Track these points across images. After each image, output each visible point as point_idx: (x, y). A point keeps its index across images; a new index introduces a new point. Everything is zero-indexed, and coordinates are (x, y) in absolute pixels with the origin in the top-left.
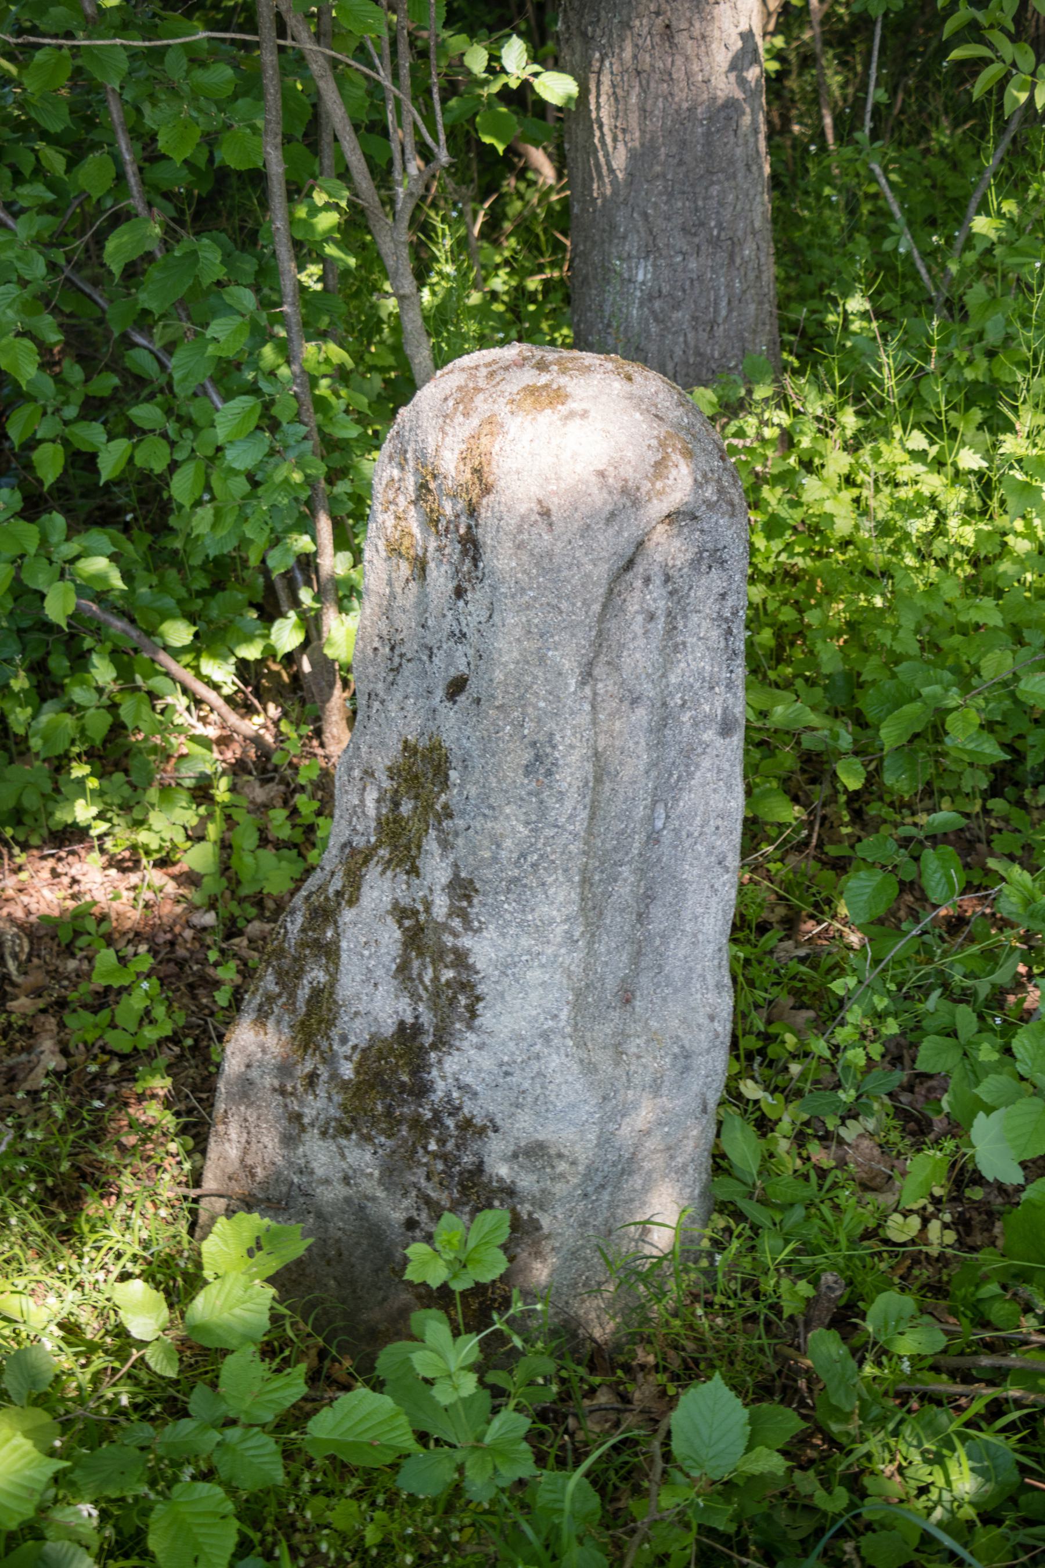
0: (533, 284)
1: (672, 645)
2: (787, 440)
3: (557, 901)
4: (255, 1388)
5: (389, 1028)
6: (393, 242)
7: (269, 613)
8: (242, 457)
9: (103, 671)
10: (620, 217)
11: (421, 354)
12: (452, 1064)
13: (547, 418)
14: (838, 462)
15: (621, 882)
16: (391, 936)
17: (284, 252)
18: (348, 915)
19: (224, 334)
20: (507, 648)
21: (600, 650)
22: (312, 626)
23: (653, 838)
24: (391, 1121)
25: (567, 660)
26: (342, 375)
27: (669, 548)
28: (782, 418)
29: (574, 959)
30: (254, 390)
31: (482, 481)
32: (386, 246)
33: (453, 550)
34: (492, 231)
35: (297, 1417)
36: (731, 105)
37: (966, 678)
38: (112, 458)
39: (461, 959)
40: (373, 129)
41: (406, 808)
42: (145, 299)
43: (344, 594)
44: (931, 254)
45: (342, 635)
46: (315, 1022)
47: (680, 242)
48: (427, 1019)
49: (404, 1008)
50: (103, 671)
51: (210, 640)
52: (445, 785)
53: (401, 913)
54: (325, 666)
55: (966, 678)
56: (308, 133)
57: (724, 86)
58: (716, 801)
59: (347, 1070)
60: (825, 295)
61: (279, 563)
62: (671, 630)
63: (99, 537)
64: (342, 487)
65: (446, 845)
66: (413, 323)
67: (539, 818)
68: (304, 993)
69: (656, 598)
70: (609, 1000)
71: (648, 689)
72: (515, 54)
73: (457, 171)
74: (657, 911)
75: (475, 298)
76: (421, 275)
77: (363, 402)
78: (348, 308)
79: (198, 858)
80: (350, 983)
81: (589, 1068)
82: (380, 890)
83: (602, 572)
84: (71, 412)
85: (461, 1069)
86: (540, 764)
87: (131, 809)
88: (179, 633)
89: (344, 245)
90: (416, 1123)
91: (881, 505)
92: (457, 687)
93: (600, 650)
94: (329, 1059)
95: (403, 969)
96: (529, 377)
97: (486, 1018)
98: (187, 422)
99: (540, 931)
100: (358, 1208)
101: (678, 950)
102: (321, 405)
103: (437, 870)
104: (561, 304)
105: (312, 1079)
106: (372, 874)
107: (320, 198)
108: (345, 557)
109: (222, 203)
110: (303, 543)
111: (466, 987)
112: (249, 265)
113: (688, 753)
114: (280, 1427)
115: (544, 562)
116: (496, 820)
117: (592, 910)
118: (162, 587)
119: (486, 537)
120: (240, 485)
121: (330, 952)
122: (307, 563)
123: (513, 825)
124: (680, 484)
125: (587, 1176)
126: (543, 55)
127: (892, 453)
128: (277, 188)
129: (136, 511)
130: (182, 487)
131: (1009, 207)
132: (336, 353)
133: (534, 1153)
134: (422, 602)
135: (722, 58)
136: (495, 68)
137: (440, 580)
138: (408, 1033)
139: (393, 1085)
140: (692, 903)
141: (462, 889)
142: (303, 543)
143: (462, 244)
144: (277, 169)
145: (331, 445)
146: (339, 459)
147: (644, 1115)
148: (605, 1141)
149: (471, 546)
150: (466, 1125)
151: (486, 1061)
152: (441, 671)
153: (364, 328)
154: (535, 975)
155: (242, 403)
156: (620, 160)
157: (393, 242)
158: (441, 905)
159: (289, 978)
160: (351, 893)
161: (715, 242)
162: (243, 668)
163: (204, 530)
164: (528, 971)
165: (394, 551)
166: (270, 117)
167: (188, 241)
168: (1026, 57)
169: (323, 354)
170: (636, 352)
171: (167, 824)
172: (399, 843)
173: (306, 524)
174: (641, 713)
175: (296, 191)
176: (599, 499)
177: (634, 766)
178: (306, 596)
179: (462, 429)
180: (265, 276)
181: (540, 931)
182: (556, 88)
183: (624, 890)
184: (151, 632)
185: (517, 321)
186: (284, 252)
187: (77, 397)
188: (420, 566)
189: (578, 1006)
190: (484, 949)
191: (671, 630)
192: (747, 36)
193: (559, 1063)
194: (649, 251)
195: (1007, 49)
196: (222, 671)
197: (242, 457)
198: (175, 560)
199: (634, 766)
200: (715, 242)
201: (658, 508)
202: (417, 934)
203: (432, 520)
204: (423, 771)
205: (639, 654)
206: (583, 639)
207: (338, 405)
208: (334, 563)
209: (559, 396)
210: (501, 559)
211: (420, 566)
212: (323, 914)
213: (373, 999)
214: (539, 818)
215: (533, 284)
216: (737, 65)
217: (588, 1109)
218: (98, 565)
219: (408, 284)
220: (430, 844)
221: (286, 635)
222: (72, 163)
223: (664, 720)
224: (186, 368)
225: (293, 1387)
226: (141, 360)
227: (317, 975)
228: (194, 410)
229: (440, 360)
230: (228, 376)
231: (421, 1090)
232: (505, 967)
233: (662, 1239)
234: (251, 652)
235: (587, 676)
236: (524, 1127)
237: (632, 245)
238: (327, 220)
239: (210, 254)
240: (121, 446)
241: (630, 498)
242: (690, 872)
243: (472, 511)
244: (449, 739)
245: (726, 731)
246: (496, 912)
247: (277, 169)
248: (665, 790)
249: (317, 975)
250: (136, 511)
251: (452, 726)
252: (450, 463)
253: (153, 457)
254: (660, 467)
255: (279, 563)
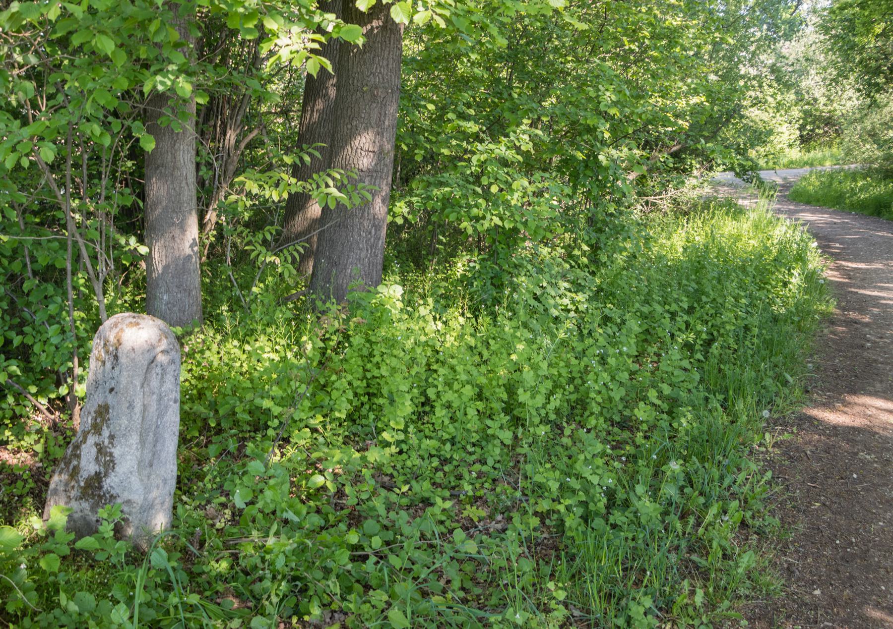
0: (138, 298)
1: (162, 382)
2: (204, 341)
3: (134, 439)
4: (62, 537)
5: (93, 473)
6: (98, 287)
7: (58, 384)
8: (55, 340)
9: (11, 399)
10: (160, 282)
11: (103, 315)
12: (108, 481)
13: (135, 329)
14: (215, 347)
15: (150, 437)
16: (94, 450)
17: (70, 289)
18: (83, 446)
19: (53, 309)
20: (124, 381)
21: (145, 381)
22: (71, 388)
23: (157, 427)
24: (93, 495)
25: (137, 382)
26: (82, 320)
27: (162, 358)
28: (202, 336)
29: (138, 454)
30: (59, 323)
31: (119, 342)
32: (96, 288)
33: (112, 358)
34: (125, 283)
35: (74, 542)
36: (190, 256)
37: (241, 400)
38: (17, 341)
39: (111, 454)
40: (94, 258)
41: (99, 420)
42: (31, 299)
43: (81, 379)
44: (244, 296)
45: (81, 389)
46: (75, 473)
47: (176, 290)
48: (102, 470)
49: (97, 468)
50: (11, 399)
51: (41, 392)
52: (108, 413)
53: (97, 445)
54: (74, 399)
55: (241, 400)
56: (77, 258)
57: (188, 251)
58: (173, 419)
59: (82, 484)
60: (216, 306)
61: (63, 369)
62: (162, 378)
63: (13, 361)
64: (81, 350)
65: (108, 427)
66: (102, 308)
67: (130, 419)
68: (71, 467)
69: (159, 370)
70: (148, 465)
71: (156, 391)
72: (133, 241)
73: (117, 269)
74: (158, 444)
75: (119, 302)
76: (105, 293)
77: (88, 328)
78: (83, 303)
79: (39, 448)
80: (83, 462)
81: (141, 480)
82: (92, 440)
83: (146, 363)
84: (6, 328)
85: (110, 482)
86: (131, 406)
87: (19, 437)
88: (33, 389)
89: (86, 286)
90: (99, 496)
91: (226, 359)
92: (112, 390)
93: (145, 381)
94: (78, 482)
95: (97, 458)
96: (131, 320)
97: (117, 469)
98: (39, 332)
99: (130, 446)
100: (84, 518)
101: (163, 455)
102: (77, 328)
103: (106, 433)
104: (142, 305)
105: (73, 487)
106: (90, 436)
107: (80, 275)
108: (81, 369)
109: (52, 275)
110: (70, 364)
111: (112, 461)
112: (61, 291)
113: (166, 407)
114: (69, 544)
115: (133, 360)
116: (121, 420)
117: (142, 442)
118: (28, 377)
119: (120, 355)
120: (53, 348)
121: (78, 457)
122: (71, 371)
123: (124, 421)
124: (164, 345)
125: (141, 507)
126: (141, 240)
127: (229, 346)
128: (69, 273)
129: (24, 354)
130: (37, 349)
131: (262, 285)
132: (83, 315)
133: (128, 502)
134: (104, 371)
135: (187, 245)
136: (127, 244)
137: (108, 365)
138: (98, 474)
139: (93, 489)
140: (167, 443)
141: (112, 437)
142: (70, 364)
143: (116, 287)
144: (69, 268)
145: (78, 338)
146: (82, 342)
147: (155, 493)
148: (145, 499)
149: (116, 357)
150: (112, 496)
151: (117, 480)
152: (108, 387)
153: (88, 309)
154: (129, 457)
155: (56, 326)
156: (160, 268)
157: (98, 287)
158: (106, 441)
159: (67, 464)
160: (84, 441)
161: (185, 290)
162: (50, 401)
163: (43, 359)
164: (127, 455)
165: (97, 359)
166: (68, 255)
167: (45, 285)
168: (264, 250)
169: (78, 314)
170: (163, 318)
171: (28, 441)
172: (97, 428)
173: (71, 359)
174: (155, 397)
175: (74, 274)
176: (146, 347)
177: (153, 408)
178: (69, 380)
179: (115, 331)
180: (65, 294)
181: (130, 446)
182: (143, 250)
183: (151, 437)
184: (26, 388)
185: (133, 307)
186: (70, 289)
187: (8, 324)
188: (104, 363)
189: (139, 465)
190: (117, 452)
191: (162, 378)
192: (194, 239)
193: (135, 479)
194: (167, 291)
195: (259, 248)
196: (44, 401)
197: (55, 340)
198: (31, 370)
199: (153, 408)
200: (185, 290)
201: (159, 349)
202: (101, 450)
203: (107, 352)
204: (103, 411)
205: (154, 383)
206: (141, 378)
207: (82, 328)
208: (78, 371)
209: (138, 324)
210: (123, 360)
211: (104, 363)
212: (77, 447)
213: (88, 465)
214: (130, 419)
215: (138, 298)
216: (191, 246)
217: (141, 491)
218: (14, 369)
219: (101, 297)
220: (105, 427)
221: (63, 390)
222: (10, 263)
223: (160, 399)
224: (39, 317)
225: (72, 536)
226: (26, 314)
227: (75, 463)
228: (41, 329)
229: (108, 317)
230: (52, 319)
231: (101, 488)
232: (121, 456)
233: (158, 528)
234: (53, 396)
235: (142, 386)
236: (126, 496)
237: (163, 290)
238: (82, 281)
239: (50, 289)
240: (20, 337)
241: (153, 347)
242: (167, 435)
243: (117, 349)
244: (109, 403)
245: (175, 402)
246: (120, 442)
247: (69, 268)
248: (161, 415)
249: (75, 463)
250: (24, 354)
251: (111, 399)
252: (112, 339)
253: (29, 341)
254: (160, 340)
255: (63, 369)
